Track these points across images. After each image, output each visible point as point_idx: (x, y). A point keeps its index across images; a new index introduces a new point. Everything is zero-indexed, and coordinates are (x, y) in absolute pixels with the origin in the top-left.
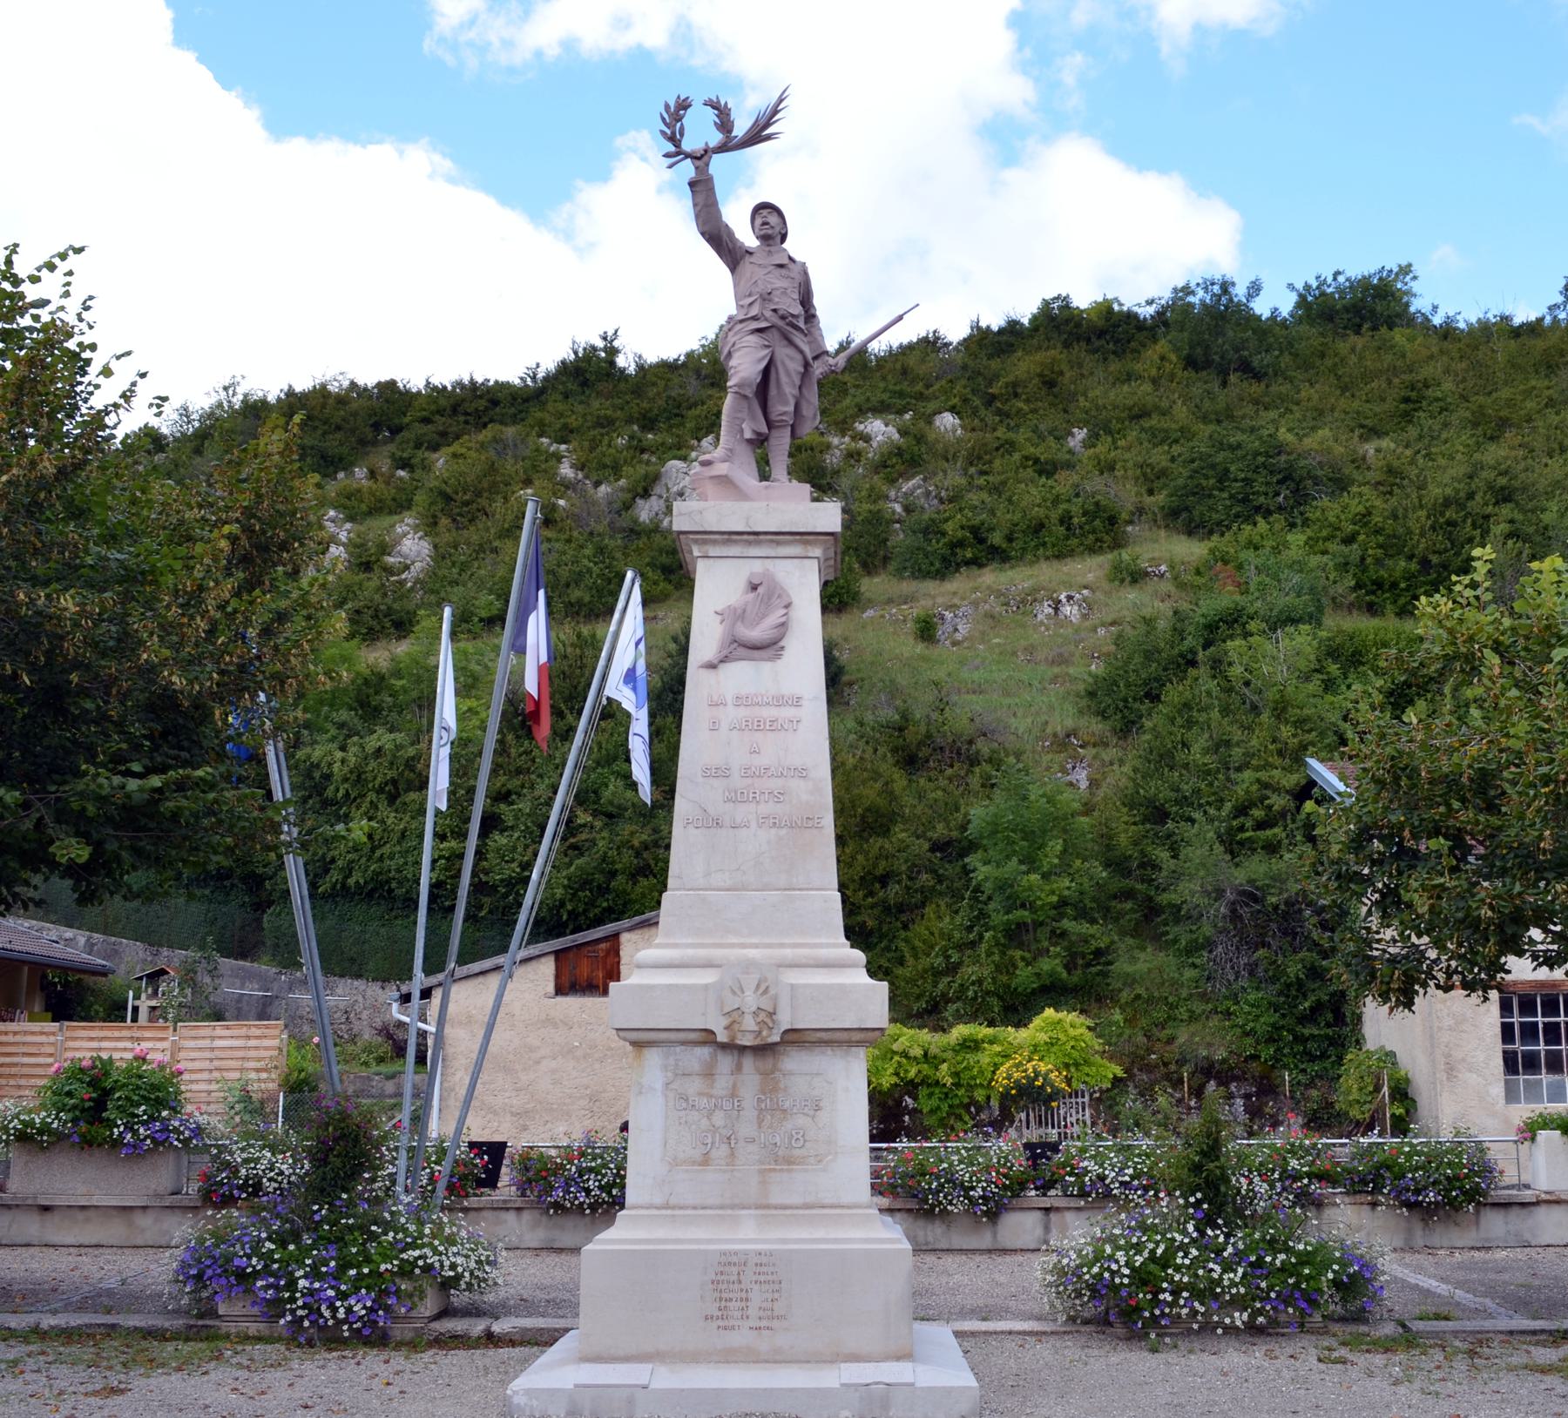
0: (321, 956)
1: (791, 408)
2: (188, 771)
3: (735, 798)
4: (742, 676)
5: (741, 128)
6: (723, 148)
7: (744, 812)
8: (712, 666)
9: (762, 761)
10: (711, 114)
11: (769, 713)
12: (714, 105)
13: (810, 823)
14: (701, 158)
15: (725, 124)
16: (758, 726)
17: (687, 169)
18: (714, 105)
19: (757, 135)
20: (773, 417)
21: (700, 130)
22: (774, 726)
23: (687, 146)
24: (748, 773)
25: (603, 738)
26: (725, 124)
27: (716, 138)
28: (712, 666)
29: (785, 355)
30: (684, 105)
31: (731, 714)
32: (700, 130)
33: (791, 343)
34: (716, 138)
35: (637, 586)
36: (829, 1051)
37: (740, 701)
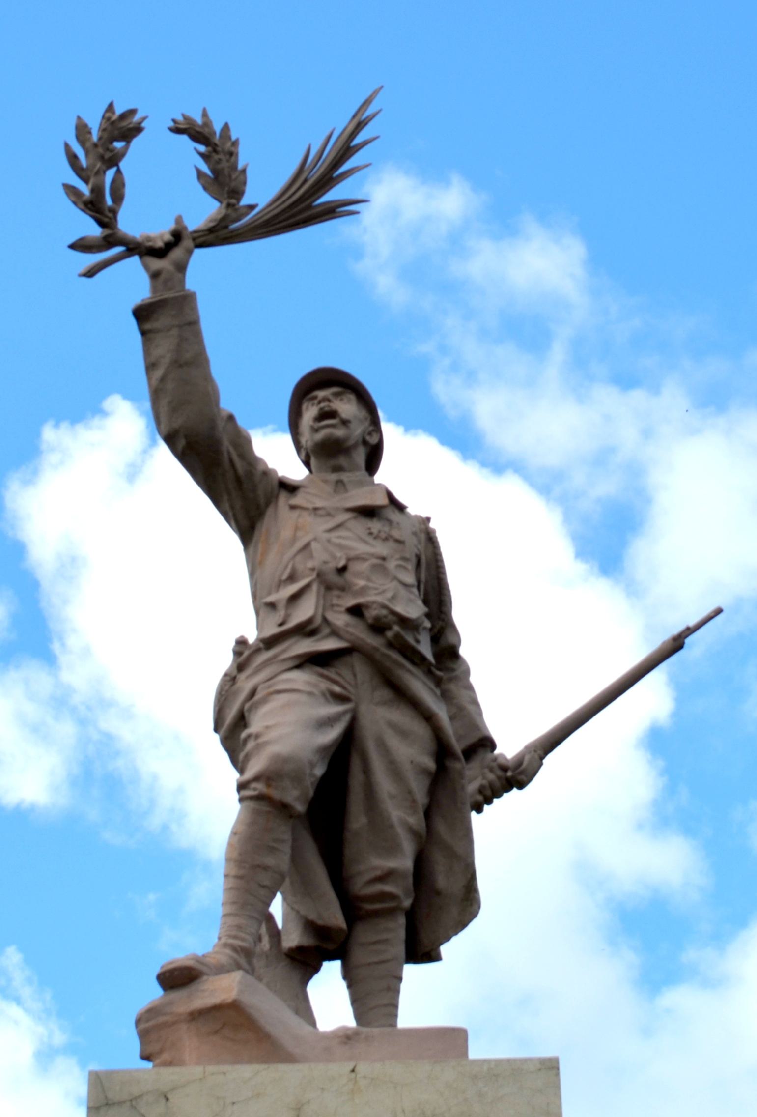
1: (405, 862)
20: (360, 887)
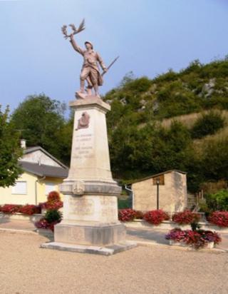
0: (45, 149)
2: (209, 137)
3: (80, 153)
4: (82, 131)
5: (77, 29)
6: (75, 33)
7: (82, 155)
8: (76, 130)
9: (85, 146)
10: (71, 28)
11: (85, 137)
12: (71, 25)
13: (77, 149)
14: (71, 36)
15: (74, 29)
16: (83, 140)
17: (69, 39)
18: (71, 25)
19: (81, 29)
21: (70, 31)
22: (86, 140)
23: (69, 34)
24: (83, 148)
25: (203, 179)
26: (74, 29)
27: (73, 32)
28: (76, 130)
29: (92, 70)
30: (65, 27)
31: (80, 138)
32: (70, 31)
33: (93, 68)
34: (73, 32)
35: (59, 166)
36: (133, 237)
37: (82, 136)
